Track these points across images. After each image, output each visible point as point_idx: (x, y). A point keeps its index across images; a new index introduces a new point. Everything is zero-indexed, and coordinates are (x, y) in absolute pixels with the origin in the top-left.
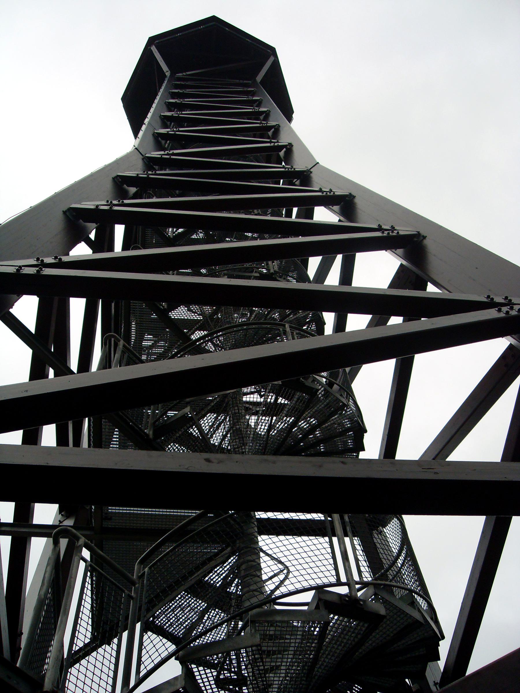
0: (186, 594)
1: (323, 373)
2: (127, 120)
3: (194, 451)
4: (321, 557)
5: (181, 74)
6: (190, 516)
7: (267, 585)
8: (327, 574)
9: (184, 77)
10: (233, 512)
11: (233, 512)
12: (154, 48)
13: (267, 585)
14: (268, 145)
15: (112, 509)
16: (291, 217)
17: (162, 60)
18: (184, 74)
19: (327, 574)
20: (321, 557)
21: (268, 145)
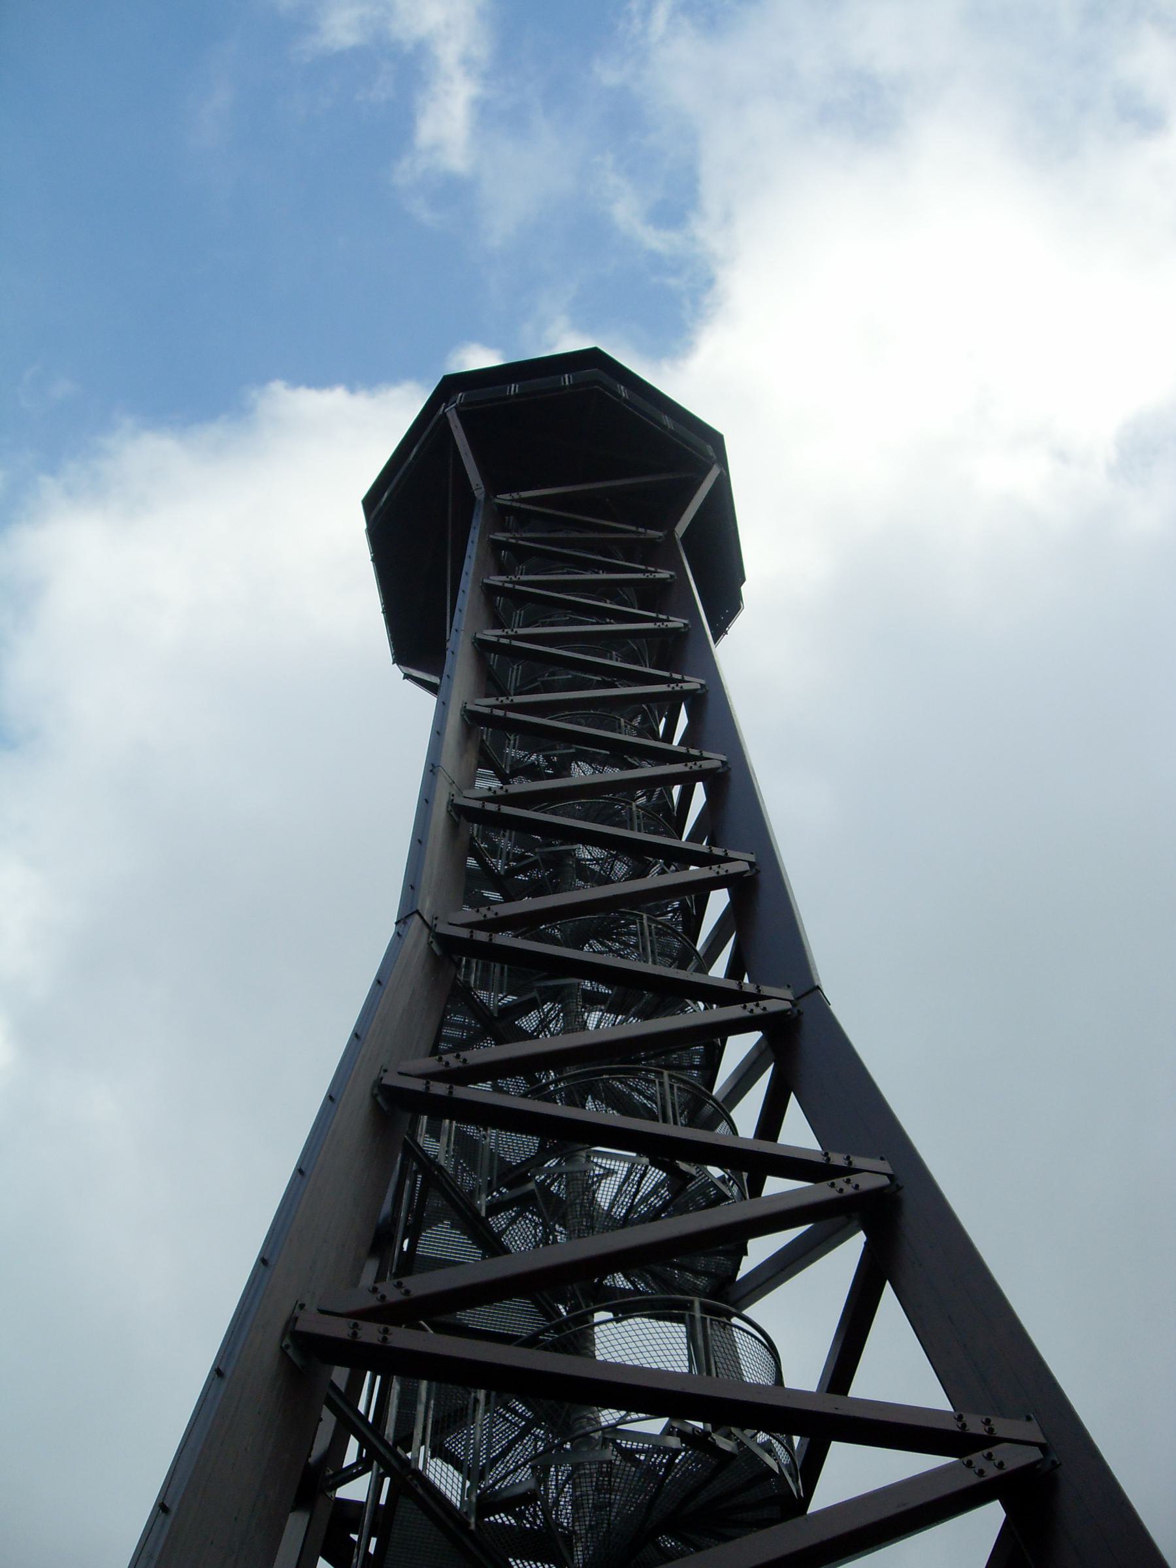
0: (524, 1413)
1: (622, 387)
2: (863, 1245)
3: (623, 1114)
4: (676, 1346)
5: (507, 496)
6: (521, 1336)
7: (603, 1416)
8: (681, 1364)
9: (514, 504)
10: (487, 1519)
11: (487, 1519)
12: (450, 412)
13: (603, 1416)
14: (651, 625)
15: (460, 1315)
16: (671, 743)
17: (470, 455)
18: (515, 495)
19: (681, 1364)
20: (676, 1346)
21: (651, 625)
